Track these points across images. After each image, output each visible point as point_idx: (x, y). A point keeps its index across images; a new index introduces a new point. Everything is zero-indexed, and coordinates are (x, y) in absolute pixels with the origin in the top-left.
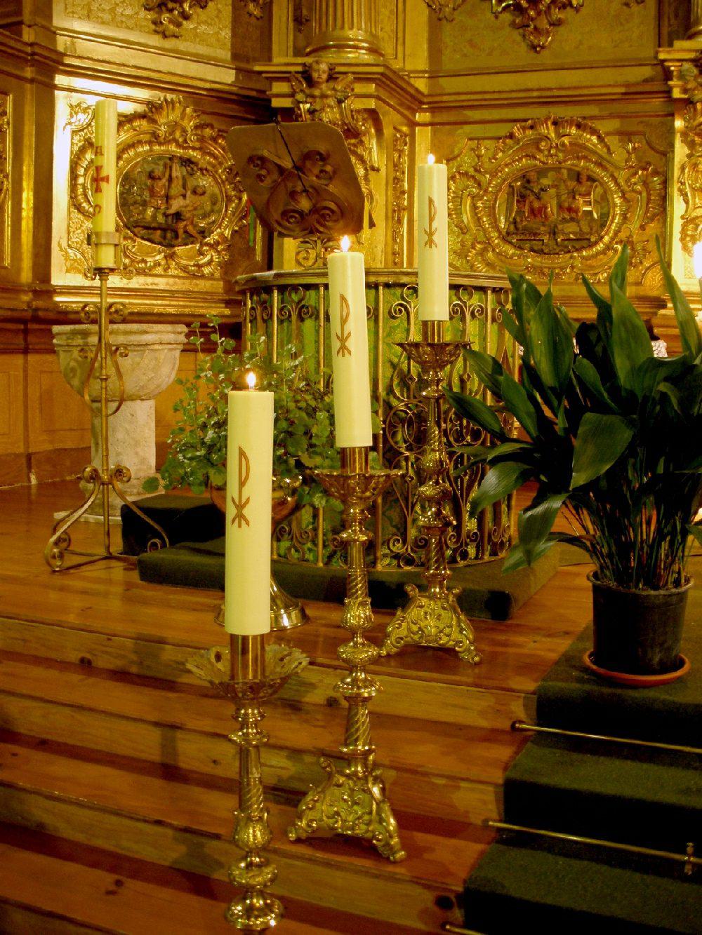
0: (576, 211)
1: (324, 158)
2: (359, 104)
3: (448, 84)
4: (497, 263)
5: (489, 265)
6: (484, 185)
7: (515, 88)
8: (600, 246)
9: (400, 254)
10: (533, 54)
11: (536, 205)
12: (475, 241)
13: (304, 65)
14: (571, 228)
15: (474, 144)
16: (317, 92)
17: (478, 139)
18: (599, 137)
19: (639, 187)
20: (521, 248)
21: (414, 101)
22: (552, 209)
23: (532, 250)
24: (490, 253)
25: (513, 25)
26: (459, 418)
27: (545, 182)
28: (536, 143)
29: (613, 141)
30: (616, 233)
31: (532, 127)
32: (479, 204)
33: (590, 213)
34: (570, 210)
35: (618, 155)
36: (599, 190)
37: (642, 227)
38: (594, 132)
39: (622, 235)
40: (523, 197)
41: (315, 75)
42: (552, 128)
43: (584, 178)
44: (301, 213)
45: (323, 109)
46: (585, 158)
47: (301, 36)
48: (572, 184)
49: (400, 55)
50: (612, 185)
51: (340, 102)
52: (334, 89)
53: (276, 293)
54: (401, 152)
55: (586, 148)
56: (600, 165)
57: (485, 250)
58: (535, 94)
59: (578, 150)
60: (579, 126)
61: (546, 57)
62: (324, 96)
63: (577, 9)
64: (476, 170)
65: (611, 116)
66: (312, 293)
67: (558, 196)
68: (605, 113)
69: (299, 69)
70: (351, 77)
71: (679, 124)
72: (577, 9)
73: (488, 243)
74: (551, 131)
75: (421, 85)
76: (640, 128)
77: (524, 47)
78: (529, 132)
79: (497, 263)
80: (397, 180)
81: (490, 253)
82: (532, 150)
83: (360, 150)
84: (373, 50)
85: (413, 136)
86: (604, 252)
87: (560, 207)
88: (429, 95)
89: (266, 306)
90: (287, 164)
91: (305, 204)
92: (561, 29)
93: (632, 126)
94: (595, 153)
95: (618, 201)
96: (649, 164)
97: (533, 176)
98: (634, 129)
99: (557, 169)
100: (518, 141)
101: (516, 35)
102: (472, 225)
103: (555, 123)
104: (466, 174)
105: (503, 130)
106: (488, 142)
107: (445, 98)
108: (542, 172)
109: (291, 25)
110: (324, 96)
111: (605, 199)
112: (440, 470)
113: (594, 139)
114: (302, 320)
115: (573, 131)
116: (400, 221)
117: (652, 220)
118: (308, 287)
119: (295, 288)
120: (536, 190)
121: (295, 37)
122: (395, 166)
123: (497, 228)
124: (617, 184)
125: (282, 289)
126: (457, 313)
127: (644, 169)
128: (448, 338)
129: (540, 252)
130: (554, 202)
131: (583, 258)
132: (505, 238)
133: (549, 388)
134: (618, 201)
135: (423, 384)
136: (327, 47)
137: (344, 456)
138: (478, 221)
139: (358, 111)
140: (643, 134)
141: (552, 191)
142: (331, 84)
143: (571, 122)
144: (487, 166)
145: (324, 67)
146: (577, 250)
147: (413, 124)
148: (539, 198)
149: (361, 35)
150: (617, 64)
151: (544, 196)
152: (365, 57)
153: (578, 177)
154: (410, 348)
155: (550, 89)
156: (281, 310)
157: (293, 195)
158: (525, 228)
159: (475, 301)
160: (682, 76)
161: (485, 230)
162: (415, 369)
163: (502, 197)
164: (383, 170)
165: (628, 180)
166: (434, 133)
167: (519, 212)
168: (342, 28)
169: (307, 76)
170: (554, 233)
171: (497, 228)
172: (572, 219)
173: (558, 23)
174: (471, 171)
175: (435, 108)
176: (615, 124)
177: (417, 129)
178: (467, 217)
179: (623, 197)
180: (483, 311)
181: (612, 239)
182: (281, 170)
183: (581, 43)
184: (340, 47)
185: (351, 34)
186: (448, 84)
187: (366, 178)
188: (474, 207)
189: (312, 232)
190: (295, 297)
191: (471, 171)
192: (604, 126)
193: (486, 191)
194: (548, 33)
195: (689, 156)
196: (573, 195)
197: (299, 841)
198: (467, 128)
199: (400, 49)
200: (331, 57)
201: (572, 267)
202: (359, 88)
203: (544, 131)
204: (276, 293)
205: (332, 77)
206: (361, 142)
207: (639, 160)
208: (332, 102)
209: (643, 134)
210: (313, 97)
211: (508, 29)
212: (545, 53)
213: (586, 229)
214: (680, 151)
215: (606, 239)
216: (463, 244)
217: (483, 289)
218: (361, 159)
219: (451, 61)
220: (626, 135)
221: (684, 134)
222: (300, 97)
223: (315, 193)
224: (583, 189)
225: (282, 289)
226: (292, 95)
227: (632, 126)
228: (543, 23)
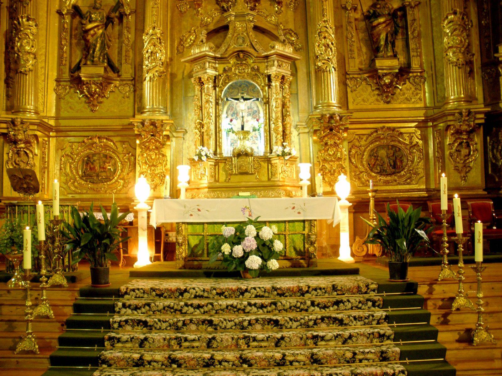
0: (106, 168)
1: (30, 176)
2: (31, 133)
3: (63, 122)
4: (78, 186)
5: (76, 187)
6: (74, 158)
7: (86, 125)
8: (114, 181)
9: (45, 184)
10: (92, 113)
11: (92, 166)
12: (71, 179)
13: (12, 118)
14: (104, 174)
15: (70, 144)
16: (16, 128)
17: (72, 142)
18: (114, 143)
19: (126, 160)
20: (86, 181)
21: (49, 128)
22: (97, 168)
23: (90, 182)
24: (76, 183)
25: (85, 102)
26: (63, 236)
27: (95, 158)
28: (92, 144)
29: (118, 145)
30: (119, 176)
31: (91, 139)
32: (72, 166)
33: (110, 169)
34: (103, 168)
35: (120, 149)
36: (113, 161)
37: (128, 174)
38: (112, 141)
39: (121, 177)
40: (87, 164)
41: (16, 123)
42: (97, 140)
43: (108, 157)
44: (24, 188)
45: (18, 135)
46: (109, 150)
47: (9, 102)
48: (104, 159)
49: (45, 111)
50: (118, 160)
51: (24, 132)
52: (22, 127)
53: (17, 207)
54: (45, 148)
55: (108, 146)
56: (113, 152)
57: (74, 182)
58: (92, 127)
59: (106, 147)
60: (107, 139)
61: (96, 114)
62: (19, 130)
63: (107, 98)
64: (72, 154)
65: (117, 136)
66: (26, 207)
67: (99, 163)
68: (116, 135)
69: (10, 120)
70: (28, 123)
71: (138, 142)
72: (107, 98)
73: (75, 180)
74: (97, 140)
75: (52, 122)
76: (127, 140)
77: (89, 110)
78: (90, 141)
79: (78, 186)
80: (43, 158)
81: (76, 183)
82: (90, 147)
83: (31, 148)
84: (37, 113)
85: (49, 141)
86: (115, 183)
87: (100, 167)
88: (55, 127)
89: (14, 210)
90: (21, 177)
91: (25, 186)
92: (102, 105)
93: (125, 139)
94: (111, 148)
95: (119, 165)
96: (130, 152)
97: (91, 156)
98: (125, 140)
99: (99, 154)
100: (86, 144)
101: (86, 106)
102: (70, 173)
103: (99, 138)
104: (67, 155)
105: (81, 139)
106: (76, 144)
107: (61, 128)
108: (94, 155)
109: (5, 97)
110: (19, 130)
111: (115, 165)
112: (58, 247)
113: (112, 144)
114: (23, 213)
115: (105, 140)
116: (44, 172)
117: (131, 171)
118: (25, 206)
119: (22, 206)
120: (92, 161)
121: (6, 102)
122: (43, 152)
123: (78, 174)
124: (119, 159)
125: (18, 206)
126: (61, 212)
127: (129, 154)
128: (59, 218)
129: (93, 183)
130: (98, 165)
131: (108, 185)
132: (81, 178)
133: (262, 227)
134: (119, 165)
135: (54, 229)
136: (19, 112)
137: (40, 242)
138: (72, 171)
139: (31, 135)
140: (128, 142)
141: (98, 161)
142: (22, 125)
143: (104, 138)
144: (75, 152)
145: (19, 120)
146: (106, 182)
147: (49, 137)
148: (93, 164)
149: (32, 107)
150: (120, 118)
151: (95, 163)
152: (34, 116)
153: (106, 156)
154: (51, 222)
155: (97, 126)
156: (18, 211)
157: (22, 184)
158: (88, 175)
159: (66, 208)
160: (138, 127)
161: (74, 175)
162: (52, 225)
163: (80, 163)
164: (39, 155)
165: (123, 158)
166: (57, 140)
167: (86, 169)
168: (25, 104)
169: (13, 122)
170: (98, 176)
171: (78, 174)
172: (104, 171)
173: (101, 102)
174: (69, 154)
175: (57, 131)
176: (119, 139)
177: (51, 139)
178: (68, 170)
179: (121, 163)
180: (68, 211)
181: (118, 178)
182: (20, 178)
183: (108, 110)
184: (25, 112)
185: (28, 107)
186: (63, 122)
187: (33, 158)
188: (71, 167)
189: (27, 192)
190: (22, 208)
191: (69, 154)
192: (115, 139)
193: (75, 161)
194: (97, 106)
195: (141, 152)
196: (104, 162)
197: (17, 354)
198: (69, 138)
199: (45, 109)
200: (20, 116)
201: (104, 188)
202: (32, 127)
203: (95, 140)
204: (17, 207)
205: (22, 123)
206: (31, 146)
207: (127, 151)
208: (22, 132)
209: (128, 142)
210: (15, 130)
211: (83, 103)
212: (96, 113)
213: (109, 175)
214: (138, 151)
215: (116, 178)
216: (66, 180)
217: (68, 206)
218: (31, 151)
219: (63, 114)
220: (123, 142)
221: (140, 145)
222: (10, 130)
223: (28, 184)
224: (108, 161)
225: (18, 206)
226: (7, 128)
227: (125, 139)
228: (95, 103)
